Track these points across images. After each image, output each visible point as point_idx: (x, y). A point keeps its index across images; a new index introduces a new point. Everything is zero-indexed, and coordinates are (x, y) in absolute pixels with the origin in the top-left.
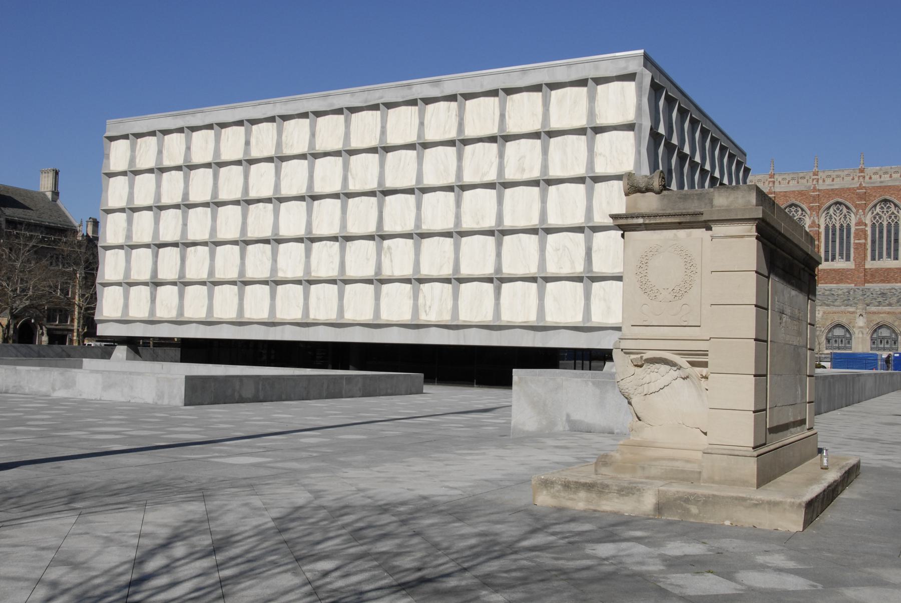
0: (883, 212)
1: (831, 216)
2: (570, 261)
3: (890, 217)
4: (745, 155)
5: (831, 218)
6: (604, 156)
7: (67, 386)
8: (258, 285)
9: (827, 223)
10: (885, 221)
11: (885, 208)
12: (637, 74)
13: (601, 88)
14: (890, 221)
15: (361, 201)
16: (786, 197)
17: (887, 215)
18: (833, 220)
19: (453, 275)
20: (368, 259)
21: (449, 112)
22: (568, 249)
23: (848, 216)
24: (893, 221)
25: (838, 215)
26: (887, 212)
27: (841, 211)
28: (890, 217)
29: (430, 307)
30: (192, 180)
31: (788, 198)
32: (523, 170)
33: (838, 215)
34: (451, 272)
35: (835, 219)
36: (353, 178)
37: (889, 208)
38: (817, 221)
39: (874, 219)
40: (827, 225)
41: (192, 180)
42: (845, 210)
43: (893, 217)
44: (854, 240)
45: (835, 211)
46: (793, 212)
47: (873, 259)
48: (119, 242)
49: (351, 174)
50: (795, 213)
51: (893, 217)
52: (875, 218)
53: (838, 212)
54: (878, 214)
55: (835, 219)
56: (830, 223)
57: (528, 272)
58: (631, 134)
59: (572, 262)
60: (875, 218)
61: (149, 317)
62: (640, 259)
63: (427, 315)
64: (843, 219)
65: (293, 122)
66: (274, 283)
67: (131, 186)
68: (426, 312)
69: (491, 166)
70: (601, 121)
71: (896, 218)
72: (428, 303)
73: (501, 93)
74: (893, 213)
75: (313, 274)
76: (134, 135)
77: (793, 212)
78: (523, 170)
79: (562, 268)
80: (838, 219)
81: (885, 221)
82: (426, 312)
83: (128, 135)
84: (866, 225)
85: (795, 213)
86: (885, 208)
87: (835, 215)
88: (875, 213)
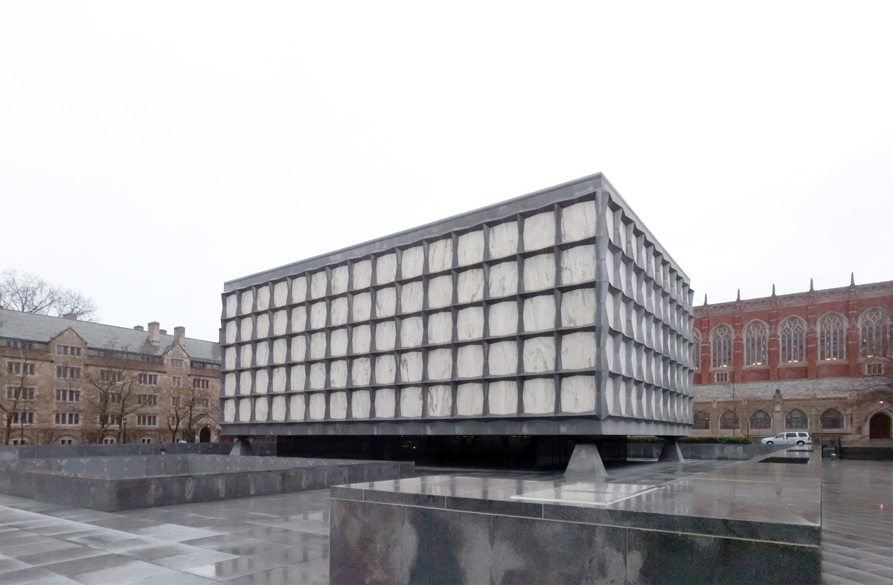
0: (791, 327)
1: (751, 332)
3: (796, 330)
4: (689, 280)
5: (825, 326)
7: (520, 492)
9: (835, 329)
10: (722, 340)
11: (792, 324)
14: (784, 334)
17: (794, 328)
18: (828, 327)
20: (391, 370)
21: (446, 248)
23: (763, 331)
24: (798, 333)
25: (756, 331)
26: (794, 326)
27: (834, 320)
28: (796, 330)
29: (436, 406)
33: (756, 331)
35: (829, 326)
36: (379, 308)
37: (795, 323)
38: (740, 336)
39: (784, 332)
40: (759, 337)
42: (761, 327)
43: (787, 331)
44: (769, 348)
45: (829, 320)
46: (874, 315)
47: (714, 366)
50: (876, 316)
51: (787, 331)
52: (785, 331)
53: (756, 328)
54: (787, 328)
55: (829, 326)
56: (825, 329)
60: (785, 331)
61: (370, 418)
64: (760, 334)
65: (338, 269)
66: (639, 381)
67: (487, 251)
68: (433, 410)
69: (479, 288)
71: (801, 331)
72: (435, 403)
73: (485, 227)
74: (798, 327)
76: (290, 277)
77: (874, 315)
80: (756, 334)
81: (722, 340)
82: (433, 410)
84: (778, 337)
85: (876, 316)
86: (792, 324)
87: (754, 331)
88: (785, 327)
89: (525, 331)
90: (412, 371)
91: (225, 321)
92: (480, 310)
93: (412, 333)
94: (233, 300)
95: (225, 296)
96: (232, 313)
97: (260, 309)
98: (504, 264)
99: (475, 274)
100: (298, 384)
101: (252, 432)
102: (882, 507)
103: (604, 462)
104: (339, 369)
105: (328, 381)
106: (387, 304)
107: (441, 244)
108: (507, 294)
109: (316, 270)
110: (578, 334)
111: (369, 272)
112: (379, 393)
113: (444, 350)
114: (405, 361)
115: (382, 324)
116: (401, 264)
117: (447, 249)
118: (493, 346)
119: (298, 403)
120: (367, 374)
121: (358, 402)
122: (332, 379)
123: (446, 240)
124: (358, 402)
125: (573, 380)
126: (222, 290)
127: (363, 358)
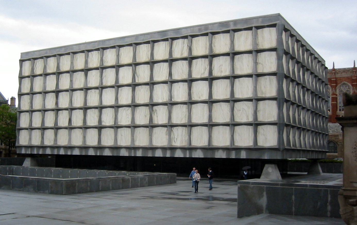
2: (246, 116)
4: (325, 61)
6: (262, 64)
8: (109, 69)
12: (277, 24)
13: (259, 31)
15: (142, 88)
16: (341, 80)
19: (188, 124)
20: (146, 116)
21: (184, 44)
22: (245, 110)
30: (60, 79)
31: (342, 81)
32: (222, 72)
34: (149, 80)
36: (138, 77)
41: (60, 79)
48: (27, 109)
49: (137, 75)
57: (225, 122)
58: (274, 53)
59: (248, 117)
62: (355, 143)
63: (175, 143)
65: (108, 50)
68: (175, 141)
69: (205, 70)
70: (260, 47)
75: (119, 144)
76: (58, 55)
78: (222, 72)
79: (242, 119)
82: (175, 141)
83: (187, 36)
89: (213, 98)
90: (50, 121)
91: (21, 78)
92: (186, 84)
93: (93, 98)
94: (27, 65)
95: (22, 61)
96: (27, 72)
97: (49, 71)
98: (221, 57)
99: (203, 62)
100: (49, 122)
101: (149, 155)
102: (29, 174)
103: (281, 174)
104: (108, 114)
105: (100, 121)
106: (65, 83)
107: (95, 53)
108: (223, 75)
109: (265, 26)
110: (267, 102)
111: (131, 54)
112: (103, 131)
113: (182, 105)
114: (156, 110)
115: (140, 87)
116: (59, 63)
117: (185, 44)
118: (120, 109)
119: (49, 134)
120: (128, 118)
121: (122, 135)
122: (102, 120)
123: (184, 39)
124: (122, 135)
125: (23, 131)
126: (19, 58)
127: (126, 108)
